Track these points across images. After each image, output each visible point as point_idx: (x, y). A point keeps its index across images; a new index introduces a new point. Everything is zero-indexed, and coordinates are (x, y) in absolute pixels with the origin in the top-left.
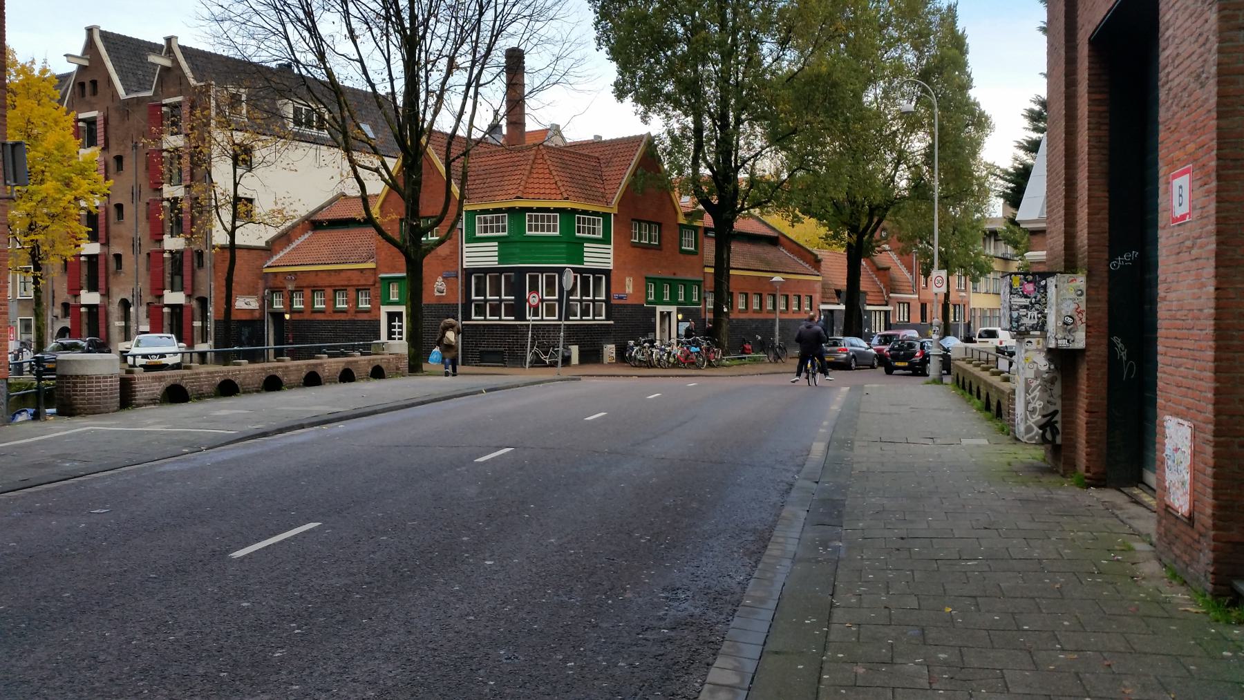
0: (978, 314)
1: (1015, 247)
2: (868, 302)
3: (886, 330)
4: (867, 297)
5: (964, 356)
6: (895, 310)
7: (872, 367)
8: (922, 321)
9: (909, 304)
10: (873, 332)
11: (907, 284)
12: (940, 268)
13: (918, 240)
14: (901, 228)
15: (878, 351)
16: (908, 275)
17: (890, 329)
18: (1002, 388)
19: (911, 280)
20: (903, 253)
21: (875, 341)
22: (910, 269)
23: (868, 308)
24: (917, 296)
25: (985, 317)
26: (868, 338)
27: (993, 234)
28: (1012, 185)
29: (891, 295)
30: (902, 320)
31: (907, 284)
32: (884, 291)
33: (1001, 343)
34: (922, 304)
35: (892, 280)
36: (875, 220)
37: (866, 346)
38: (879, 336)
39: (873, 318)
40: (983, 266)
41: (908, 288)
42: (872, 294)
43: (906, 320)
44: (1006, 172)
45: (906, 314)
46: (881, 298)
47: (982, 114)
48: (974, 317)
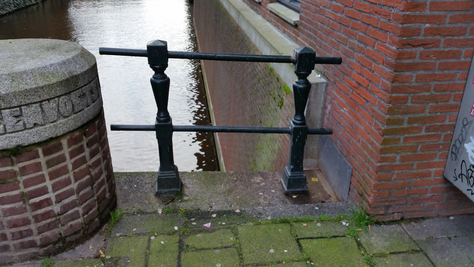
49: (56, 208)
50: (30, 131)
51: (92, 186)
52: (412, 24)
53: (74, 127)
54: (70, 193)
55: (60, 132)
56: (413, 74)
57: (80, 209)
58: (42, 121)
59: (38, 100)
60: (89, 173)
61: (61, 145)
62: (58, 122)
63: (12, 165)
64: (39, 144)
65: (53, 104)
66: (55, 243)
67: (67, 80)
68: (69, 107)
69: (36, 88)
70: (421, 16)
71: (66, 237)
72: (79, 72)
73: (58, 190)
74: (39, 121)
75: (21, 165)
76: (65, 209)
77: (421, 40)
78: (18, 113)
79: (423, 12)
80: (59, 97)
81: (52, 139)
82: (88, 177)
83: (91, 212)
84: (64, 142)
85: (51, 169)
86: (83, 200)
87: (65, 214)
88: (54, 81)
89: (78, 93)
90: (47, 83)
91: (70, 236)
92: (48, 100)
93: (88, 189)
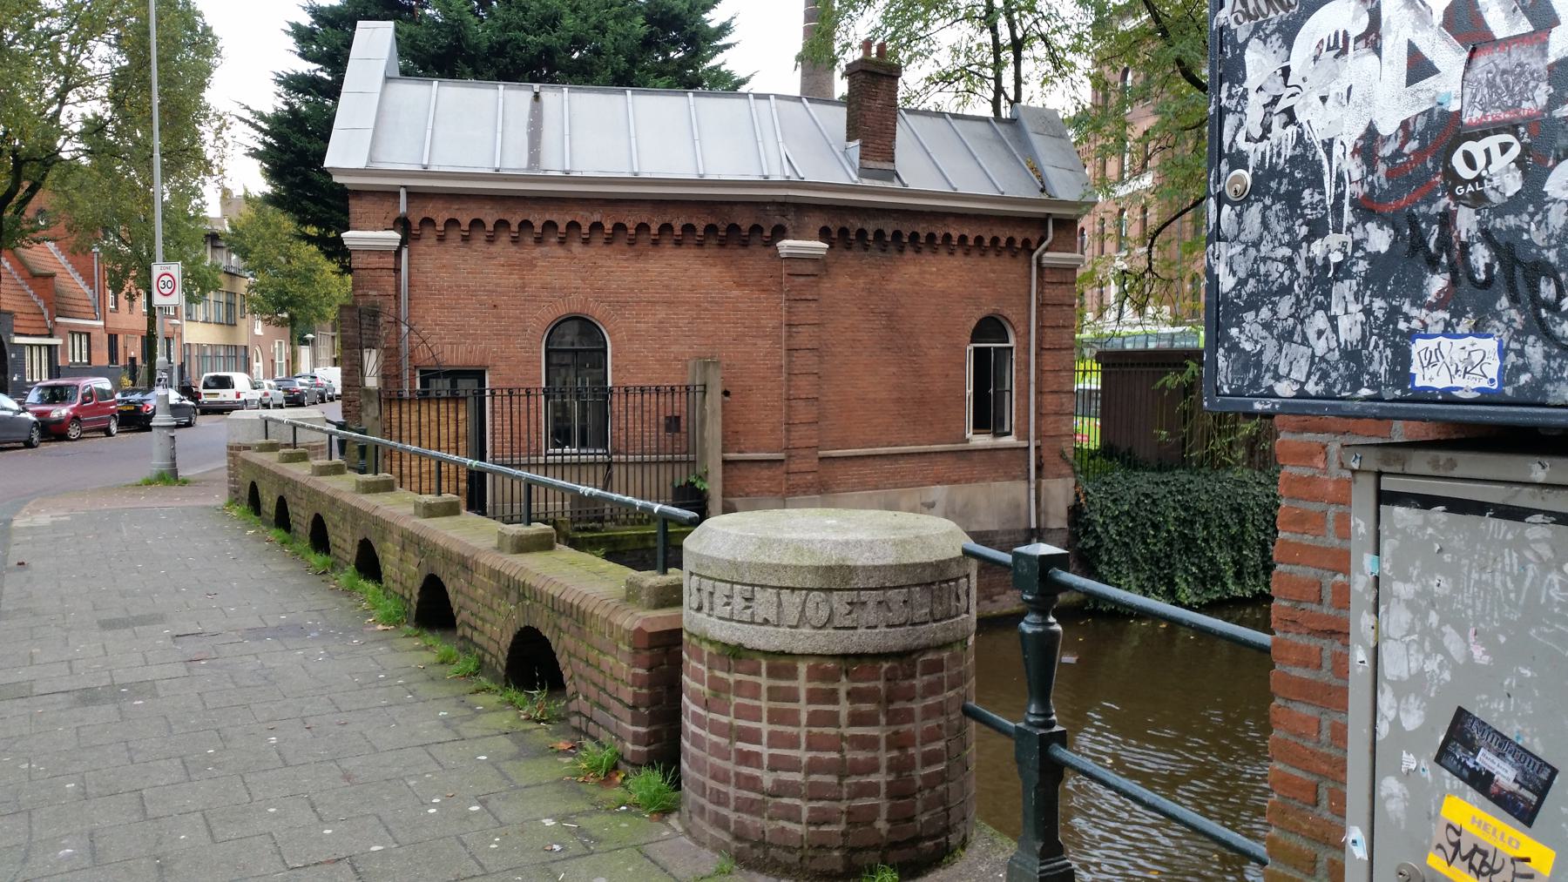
0: (195, 352)
1: (244, 257)
2: (16, 330)
3: (50, 377)
4: (16, 322)
5: (263, 441)
6: (65, 346)
7: (29, 444)
8: (111, 362)
9: (88, 335)
10: (29, 380)
11: (85, 303)
12: (168, 258)
13: (101, 234)
14: (72, 206)
15: (39, 414)
16: (86, 290)
17: (58, 376)
18: (288, 475)
19: (90, 297)
20: (77, 253)
21: (33, 397)
22: (89, 279)
23: (18, 340)
24: (102, 323)
25: (204, 356)
26: (19, 392)
27: (213, 238)
28: (269, 139)
29: (59, 320)
30: (77, 360)
31: (85, 303)
32: (46, 313)
33: (238, 396)
34: (110, 336)
35: (59, 295)
36: (26, 184)
37: (15, 406)
38: (40, 387)
39: (28, 357)
40: (206, 279)
41: (86, 310)
42: (24, 316)
43: (85, 360)
44: (262, 117)
45: (84, 352)
46: (41, 324)
47: (207, 30)
48: (189, 356)
49: (768, 779)
50: (758, 627)
51: (841, 777)
52: (1299, 568)
53: (824, 650)
54: (793, 766)
55: (798, 648)
56: (1323, 717)
57: (805, 807)
58: (775, 618)
59: (776, 583)
60: (841, 751)
61: (795, 669)
62: (798, 631)
63: (729, 671)
64: (766, 653)
65: (797, 598)
66: (754, 845)
67: (830, 569)
68: (824, 613)
69: (778, 565)
70: (1314, 547)
71: (772, 845)
72: (859, 563)
73: (776, 747)
74: (772, 618)
75: (739, 677)
76: (781, 790)
77: (1328, 618)
78: (748, 595)
79: (1320, 539)
80: (810, 590)
81: (782, 653)
82: (835, 755)
83: (824, 828)
84: (802, 668)
85: (773, 704)
86: (814, 793)
87: (778, 800)
88: (807, 562)
89: (847, 596)
90: (794, 563)
91: (778, 847)
92: (793, 589)
93: (831, 779)
